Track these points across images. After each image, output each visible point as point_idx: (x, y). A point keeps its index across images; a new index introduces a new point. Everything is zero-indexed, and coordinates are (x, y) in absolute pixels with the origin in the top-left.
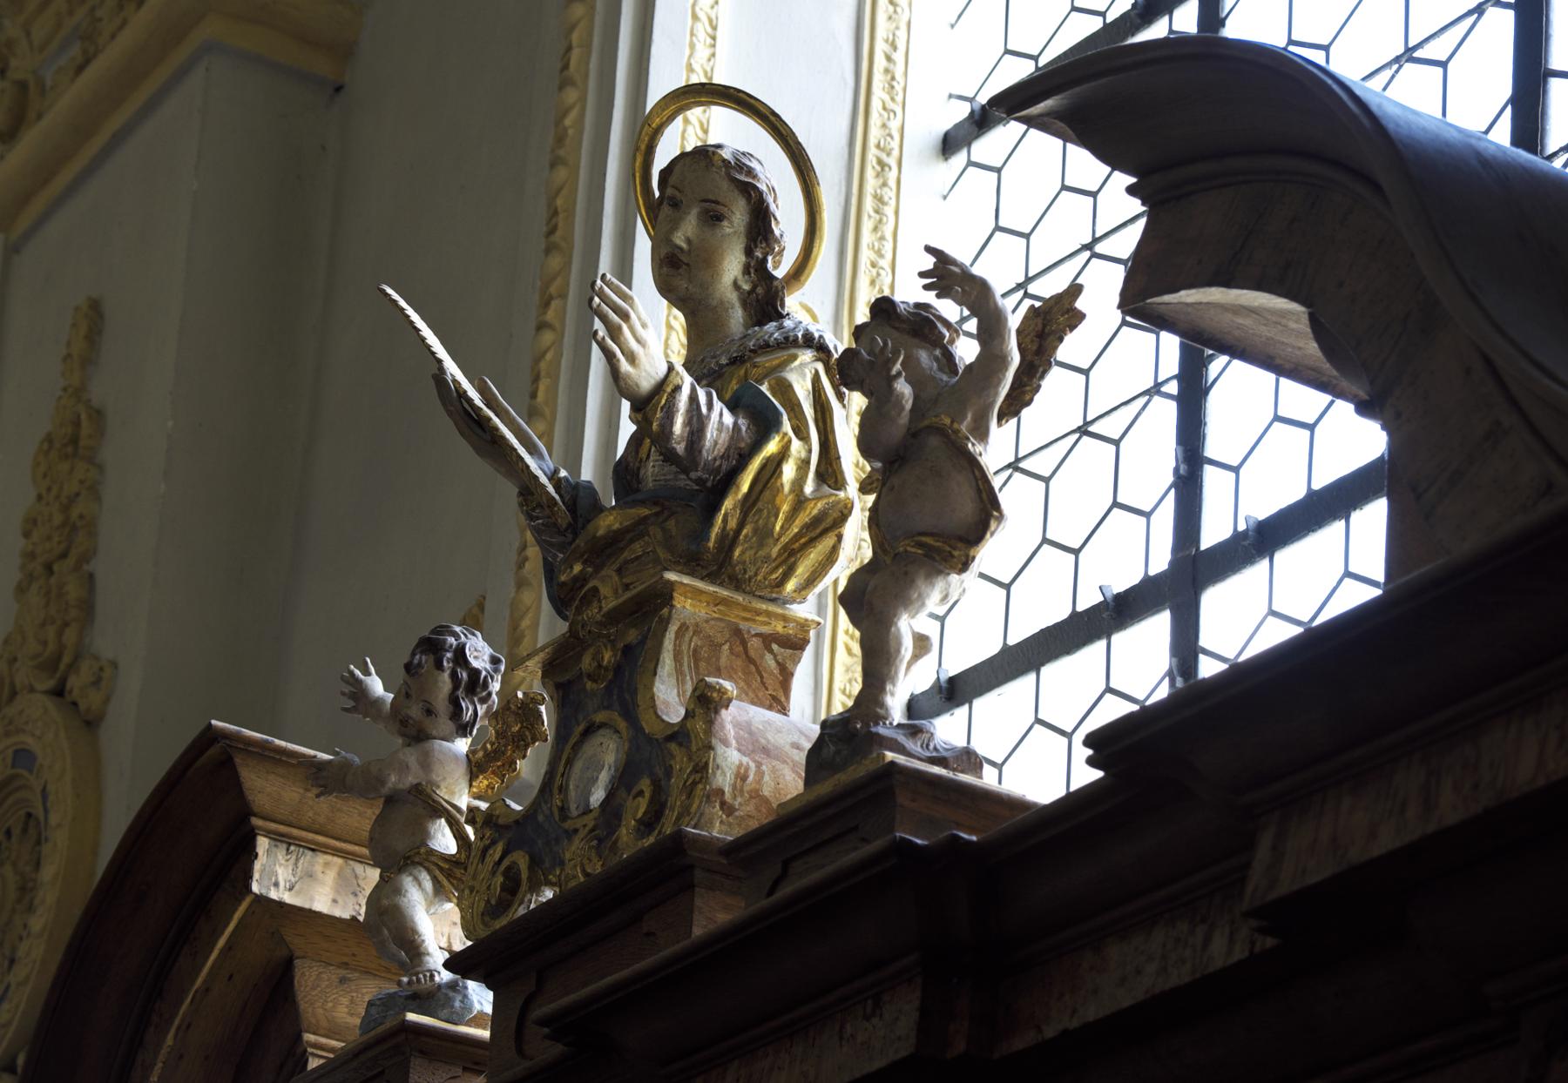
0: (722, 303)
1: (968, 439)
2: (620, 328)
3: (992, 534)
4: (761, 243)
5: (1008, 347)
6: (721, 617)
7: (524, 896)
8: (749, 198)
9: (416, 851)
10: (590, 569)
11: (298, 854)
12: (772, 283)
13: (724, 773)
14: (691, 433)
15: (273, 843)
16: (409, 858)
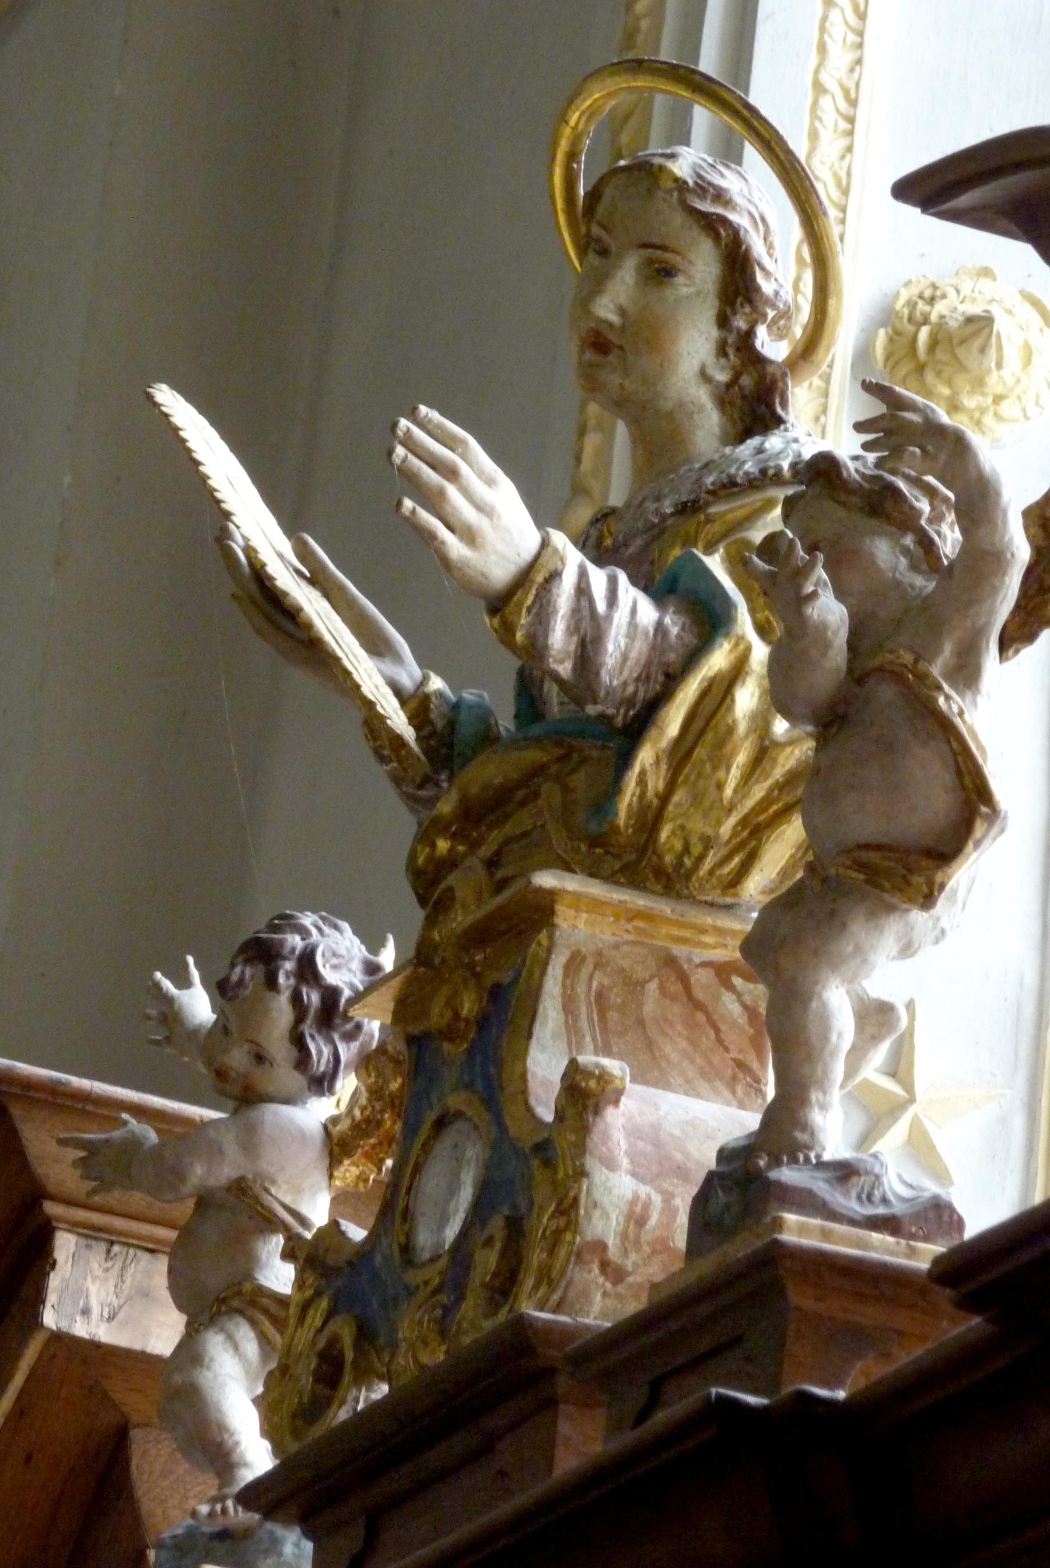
0: (681, 404)
1: (939, 688)
2: (441, 493)
3: (977, 844)
4: (742, 306)
5: (1003, 536)
6: (639, 939)
7: (347, 1391)
8: (717, 237)
9: (236, 1288)
10: (461, 848)
11: (124, 1262)
12: (764, 369)
13: (606, 1216)
14: (583, 644)
15: (83, 1242)
16: (224, 1300)
